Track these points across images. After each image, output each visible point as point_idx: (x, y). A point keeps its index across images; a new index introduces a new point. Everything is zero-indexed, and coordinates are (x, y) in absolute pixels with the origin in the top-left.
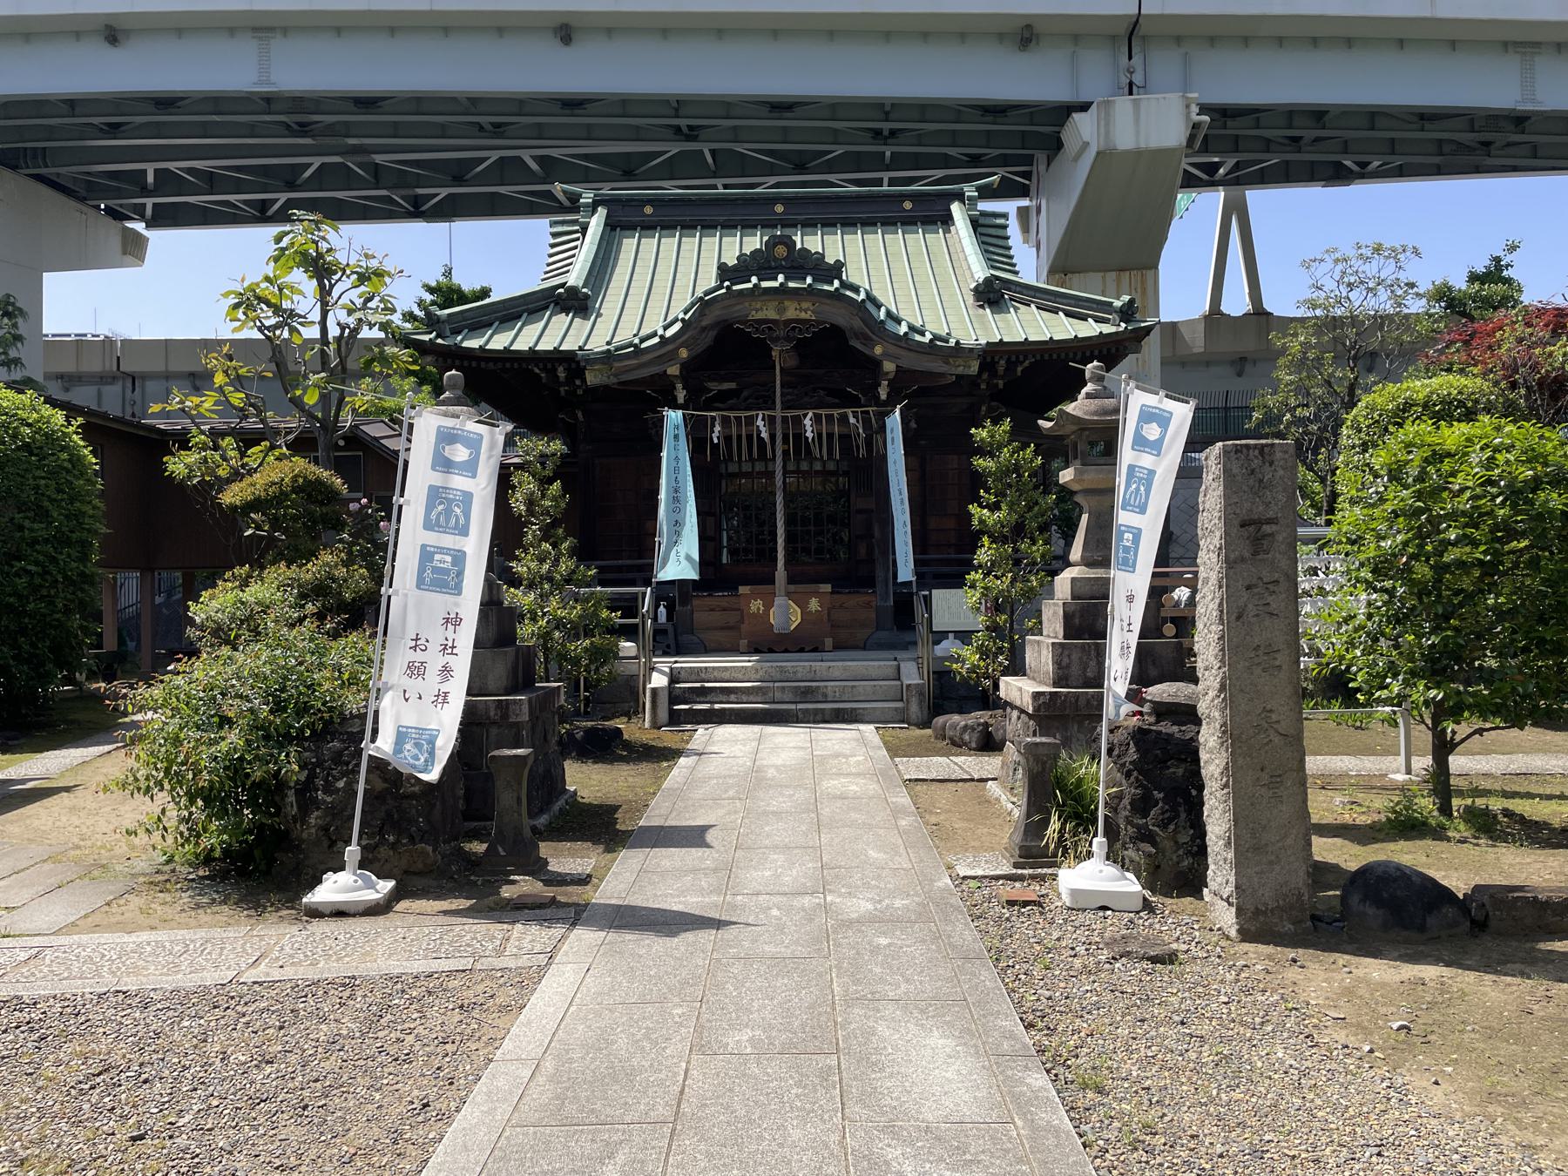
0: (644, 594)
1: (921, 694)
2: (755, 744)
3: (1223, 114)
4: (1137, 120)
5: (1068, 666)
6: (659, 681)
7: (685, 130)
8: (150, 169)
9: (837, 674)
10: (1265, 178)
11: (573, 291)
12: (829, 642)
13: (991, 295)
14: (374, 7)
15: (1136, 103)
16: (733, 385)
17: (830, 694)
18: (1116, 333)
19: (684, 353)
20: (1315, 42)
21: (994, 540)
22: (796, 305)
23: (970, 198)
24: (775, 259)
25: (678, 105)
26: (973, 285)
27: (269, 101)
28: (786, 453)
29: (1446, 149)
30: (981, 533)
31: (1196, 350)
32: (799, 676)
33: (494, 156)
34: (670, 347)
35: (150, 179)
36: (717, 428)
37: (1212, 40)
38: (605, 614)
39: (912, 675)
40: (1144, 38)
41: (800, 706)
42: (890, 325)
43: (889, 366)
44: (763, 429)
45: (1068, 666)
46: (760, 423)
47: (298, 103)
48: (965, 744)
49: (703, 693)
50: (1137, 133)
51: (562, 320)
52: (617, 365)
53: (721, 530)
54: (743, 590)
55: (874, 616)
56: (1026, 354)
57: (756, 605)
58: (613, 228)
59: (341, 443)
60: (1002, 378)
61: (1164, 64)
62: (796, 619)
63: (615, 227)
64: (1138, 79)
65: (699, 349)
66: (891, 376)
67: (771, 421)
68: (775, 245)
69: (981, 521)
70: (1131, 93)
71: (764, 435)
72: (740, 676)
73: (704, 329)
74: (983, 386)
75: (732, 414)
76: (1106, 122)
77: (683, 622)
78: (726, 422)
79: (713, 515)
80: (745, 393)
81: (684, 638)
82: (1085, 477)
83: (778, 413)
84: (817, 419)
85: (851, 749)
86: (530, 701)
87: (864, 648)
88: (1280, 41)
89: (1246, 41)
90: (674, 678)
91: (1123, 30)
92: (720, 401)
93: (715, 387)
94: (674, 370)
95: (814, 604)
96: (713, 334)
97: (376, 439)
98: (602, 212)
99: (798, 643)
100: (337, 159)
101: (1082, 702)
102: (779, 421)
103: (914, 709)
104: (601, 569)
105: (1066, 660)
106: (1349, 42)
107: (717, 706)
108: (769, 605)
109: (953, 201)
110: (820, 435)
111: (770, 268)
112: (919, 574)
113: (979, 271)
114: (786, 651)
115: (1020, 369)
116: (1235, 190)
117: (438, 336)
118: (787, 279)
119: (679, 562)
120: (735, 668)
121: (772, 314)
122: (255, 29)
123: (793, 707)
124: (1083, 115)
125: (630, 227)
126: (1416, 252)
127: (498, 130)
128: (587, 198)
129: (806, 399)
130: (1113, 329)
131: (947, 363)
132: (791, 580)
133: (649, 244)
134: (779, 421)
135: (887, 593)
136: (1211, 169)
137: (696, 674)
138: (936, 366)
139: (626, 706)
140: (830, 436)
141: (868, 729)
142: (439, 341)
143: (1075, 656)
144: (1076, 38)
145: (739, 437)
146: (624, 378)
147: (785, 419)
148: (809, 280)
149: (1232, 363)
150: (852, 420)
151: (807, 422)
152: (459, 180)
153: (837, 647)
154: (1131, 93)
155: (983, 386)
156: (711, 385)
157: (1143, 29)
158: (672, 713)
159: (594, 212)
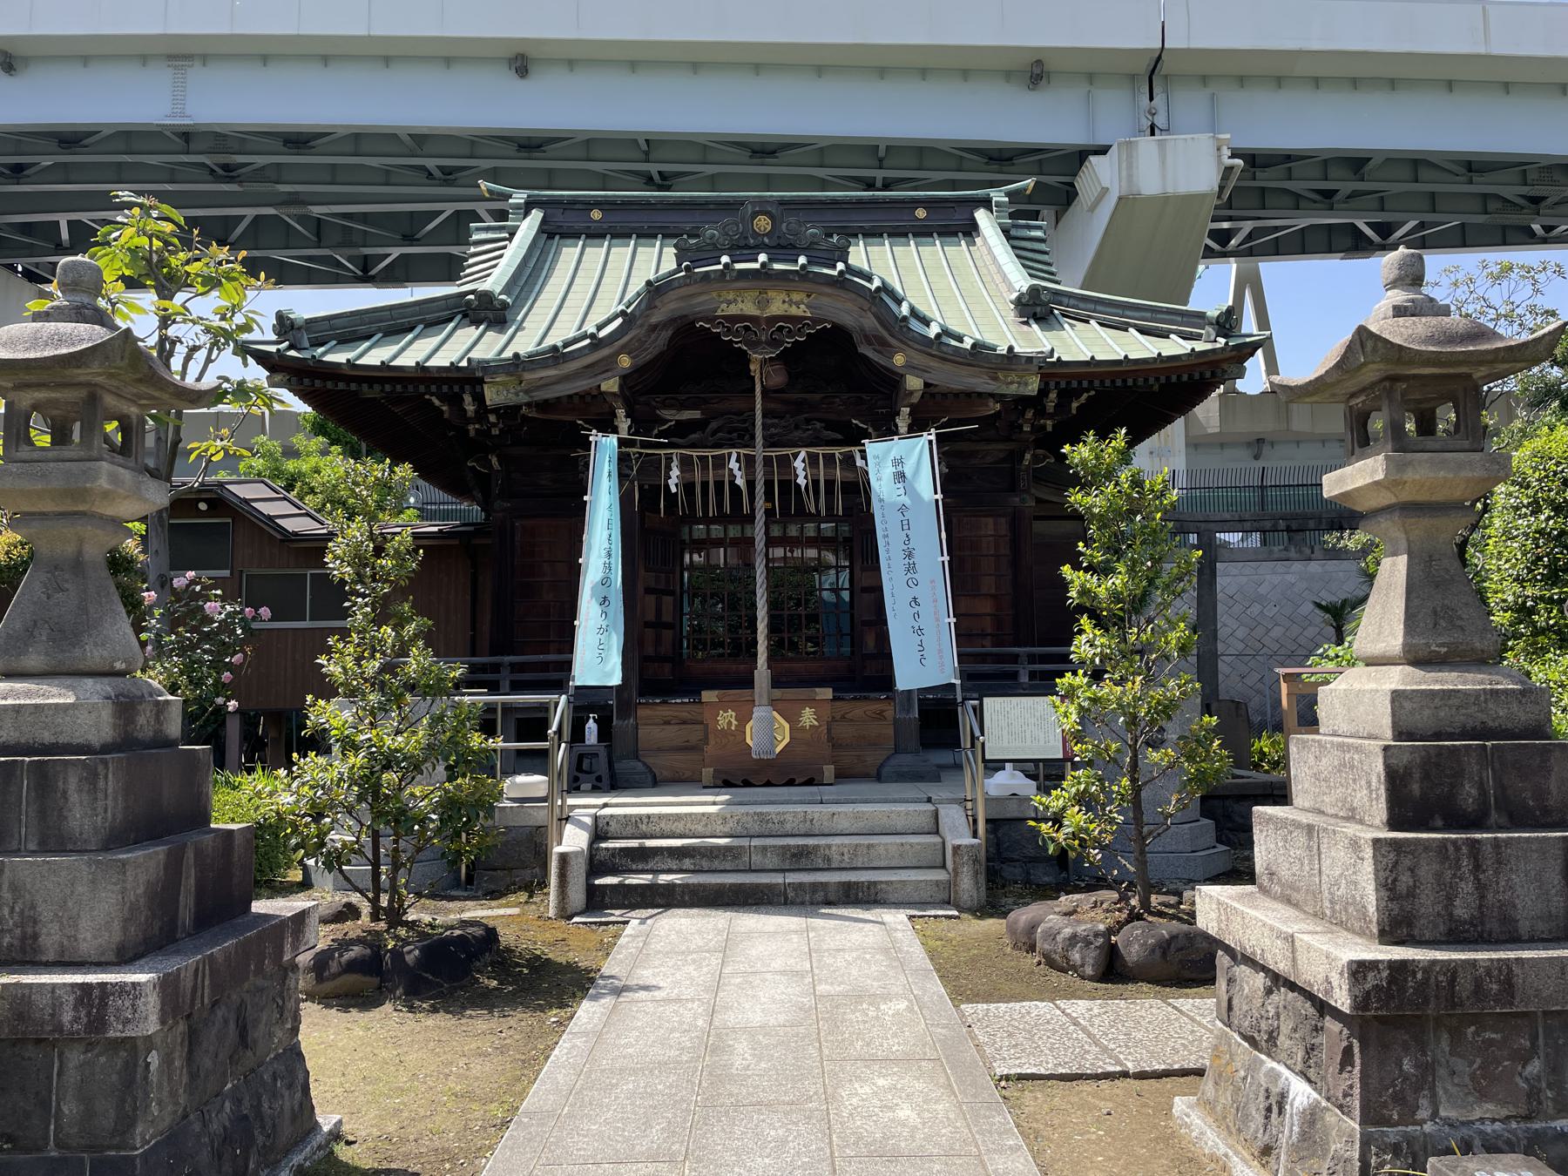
0: (557, 704)
1: (976, 861)
2: (715, 961)
3: (1255, 160)
5: (1411, 894)
6: (574, 840)
7: (656, 177)
8: (63, 220)
9: (843, 825)
10: (1281, 248)
11: (486, 297)
12: (829, 771)
13: (1035, 308)
15: (1161, 143)
16: (695, 414)
17: (836, 858)
18: (1213, 351)
19: (625, 362)
20: (1355, 83)
21: (1100, 623)
22: (783, 296)
23: (998, 204)
24: (755, 235)
25: (650, 145)
26: (1014, 296)
27: (186, 136)
28: (769, 513)
29: (1492, 206)
30: (1081, 609)
31: (1210, 431)
32: (788, 827)
33: (449, 208)
34: (605, 352)
35: (65, 235)
36: (675, 472)
37: (1242, 81)
38: (476, 740)
39: (959, 833)
41: (792, 878)
42: (915, 325)
43: (914, 383)
45: (1411, 894)
46: (733, 465)
47: (221, 139)
48: (1074, 968)
49: (643, 854)
50: (1164, 177)
51: (470, 333)
52: (527, 376)
53: (682, 614)
54: (708, 696)
55: (891, 731)
56: (1091, 377)
57: (726, 719)
58: (551, 236)
59: (203, 506)
60: (1051, 416)
61: (1187, 103)
62: (783, 740)
63: (551, 233)
64: (1160, 121)
65: (646, 357)
66: (915, 399)
67: (749, 462)
69: (1084, 592)
70: (1153, 134)
71: (740, 481)
72: (700, 828)
73: (654, 328)
74: (1027, 428)
75: (695, 453)
76: (1130, 163)
77: (611, 751)
78: (686, 463)
79: (672, 593)
80: (714, 425)
81: (622, 766)
82: (1410, 475)
83: (759, 452)
84: (812, 460)
85: (873, 953)
86: (168, 986)
87: (879, 778)
88: (1317, 82)
89: (1279, 81)
90: (599, 832)
91: (1143, 67)
92: (680, 434)
93: (672, 416)
94: (611, 385)
95: (808, 717)
97: (246, 501)
98: (536, 215)
100: (271, 211)
101: (1465, 986)
103: (969, 885)
104: (473, 668)
105: (1405, 880)
106: (1393, 84)
107: (664, 878)
108: (744, 719)
109: (977, 207)
110: (816, 483)
111: (747, 247)
112: (966, 676)
113: (1021, 281)
114: (768, 784)
115: (1075, 405)
116: (1248, 262)
117: (291, 347)
118: (771, 260)
119: (598, 657)
120: (693, 810)
121: (747, 307)
123: (777, 879)
124: (1101, 157)
125: (571, 235)
126: (1559, 272)
127: (449, 175)
128: (519, 197)
129: (797, 434)
130: (1209, 346)
131: (996, 379)
132: (776, 683)
133: (595, 253)
136: (1222, 237)
137: (635, 826)
138: (982, 383)
139: (526, 874)
140: (830, 484)
141: (897, 918)
142: (292, 353)
143: (1426, 871)
144: (1091, 77)
145: (705, 485)
147: (768, 461)
148: (802, 260)
149: (1249, 445)
151: (799, 464)
152: (409, 239)
153: (843, 776)
154: (1153, 134)
155: (1027, 428)
156: (666, 414)
157: (1165, 68)
158: (592, 890)
159: (526, 214)
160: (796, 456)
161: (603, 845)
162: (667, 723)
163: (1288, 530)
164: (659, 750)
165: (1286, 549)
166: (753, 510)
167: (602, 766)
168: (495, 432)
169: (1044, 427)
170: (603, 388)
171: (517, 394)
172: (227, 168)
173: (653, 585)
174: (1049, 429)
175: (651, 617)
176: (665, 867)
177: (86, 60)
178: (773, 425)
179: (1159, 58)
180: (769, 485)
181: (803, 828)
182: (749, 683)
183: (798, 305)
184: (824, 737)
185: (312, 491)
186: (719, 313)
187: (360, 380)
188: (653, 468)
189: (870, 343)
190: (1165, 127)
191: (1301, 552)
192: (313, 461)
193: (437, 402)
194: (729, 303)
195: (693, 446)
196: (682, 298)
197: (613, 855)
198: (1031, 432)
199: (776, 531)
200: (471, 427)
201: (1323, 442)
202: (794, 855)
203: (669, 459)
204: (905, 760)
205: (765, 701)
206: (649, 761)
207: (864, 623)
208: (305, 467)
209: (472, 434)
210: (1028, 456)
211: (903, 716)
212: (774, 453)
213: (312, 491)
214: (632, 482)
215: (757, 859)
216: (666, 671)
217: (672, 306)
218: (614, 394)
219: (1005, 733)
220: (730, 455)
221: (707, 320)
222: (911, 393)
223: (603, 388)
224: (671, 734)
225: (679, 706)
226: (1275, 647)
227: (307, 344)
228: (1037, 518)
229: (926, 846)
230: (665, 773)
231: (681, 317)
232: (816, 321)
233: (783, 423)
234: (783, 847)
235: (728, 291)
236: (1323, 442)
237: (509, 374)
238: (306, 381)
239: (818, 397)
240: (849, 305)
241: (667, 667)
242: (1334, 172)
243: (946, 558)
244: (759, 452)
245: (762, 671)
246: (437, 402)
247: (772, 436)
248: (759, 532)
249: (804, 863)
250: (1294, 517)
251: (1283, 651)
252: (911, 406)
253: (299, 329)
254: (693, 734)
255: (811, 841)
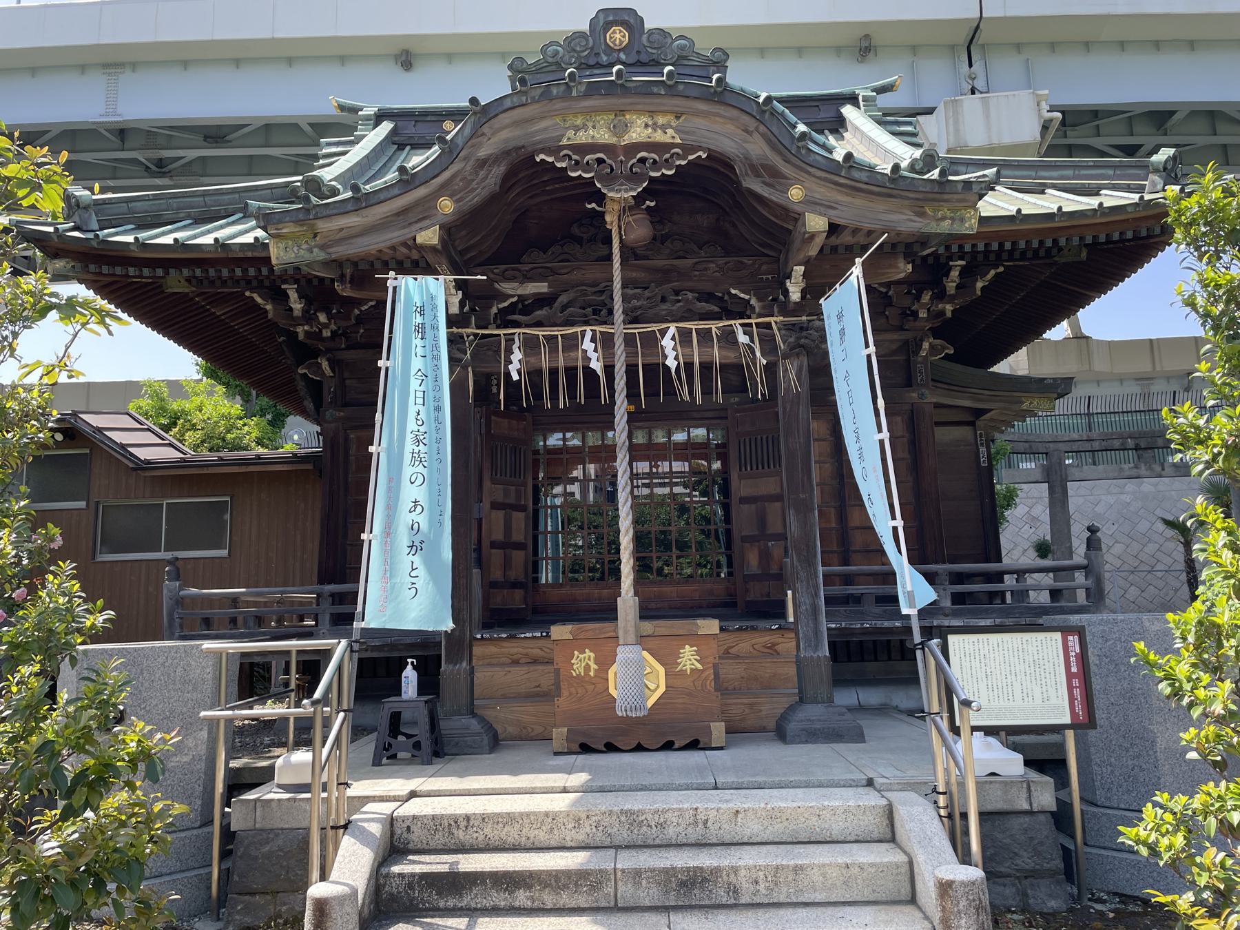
3: (1073, 117)
4: (987, 116)
9: (752, 828)
12: (718, 730)
14: (218, 36)
15: (985, 102)
16: (542, 288)
17: (746, 886)
19: (447, 206)
20: (1157, 45)
22: (646, 119)
23: (865, 99)
24: (609, 50)
27: (122, 133)
32: (671, 833)
36: (517, 356)
37: (1053, 46)
40: (983, 46)
43: (816, 223)
44: (593, 356)
46: (588, 345)
52: (323, 226)
54: (560, 632)
55: (792, 671)
57: (583, 661)
58: (401, 147)
60: (952, 299)
61: (1006, 67)
62: (657, 685)
64: (980, 84)
65: (476, 197)
67: (606, 343)
68: (608, 25)
70: (973, 93)
72: (542, 836)
73: (482, 163)
74: (923, 314)
75: (540, 332)
78: (530, 345)
79: (523, 508)
80: (563, 299)
81: (452, 725)
83: (618, 328)
84: (684, 338)
87: (781, 734)
89: (1087, 46)
90: (395, 845)
91: (963, 36)
93: (514, 290)
95: (689, 658)
96: (499, 170)
98: (386, 127)
99: (666, 734)
102: (619, 342)
108: (605, 661)
109: (843, 104)
114: (639, 748)
115: (979, 285)
117: (75, 229)
119: (406, 583)
122: (106, 66)
131: (922, 214)
132: (646, 613)
134: (619, 342)
135: (816, 632)
137: (452, 835)
140: (706, 367)
142: (76, 234)
144: (914, 49)
145: (554, 372)
146: (339, 251)
147: (629, 340)
150: (743, 339)
151: (667, 343)
156: (507, 287)
157: (982, 38)
159: (376, 125)
160: (663, 333)
161: (396, 869)
162: (516, 662)
163: (1137, 448)
164: (505, 697)
165: (1136, 467)
166: (613, 402)
167: (421, 731)
168: (326, 333)
169: (943, 313)
170: (419, 240)
171: (310, 250)
172: (160, 163)
173: (500, 499)
174: (949, 314)
175: (499, 536)
176: (487, 903)
177: (33, 71)
178: (635, 297)
179: (978, 27)
180: (631, 370)
181: (693, 835)
182: (608, 612)
183: (664, 128)
184: (710, 685)
185: (194, 427)
186: (565, 142)
187: (153, 263)
188: (490, 350)
189: (758, 175)
190: (985, 89)
191: (1150, 469)
192: (197, 400)
193: (259, 300)
194: (577, 129)
195: (538, 324)
196: (516, 124)
197: (411, 886)
198: (927, 320)
199: (640, 438)
200: (300, 329)
201: (1121, 381)
202: (682, 884)
203: (510, 340)
204: (813, 713)
205: (632, 637)
206: (489, 714)
207: (744, 539)
208: (188, 406)
209: (301, 337)
210: (926, 345)
211: (810, 654)
212: (637, 329)
213: (194, 427)
214: (465, 368)
215: (626, 892)
216: (516, 599)
217: (505, 134)
218: (433, 248)
219: (982, 686)
220: (583, 333)
221: (548, 151)
222: (813, 236)
223: (419, 240)
224: (519, 678)
225: (527, 641)
226: (1118, 563)
227: (96, 227)
228: (938, 424)
229: (882, 868)
230: (510, 729)
231: (518, 149)
232: (688, 149)
233: (647, 293)
234: (666, 871)
235: (575, 114)
236: (1121, 381)
237: (298, 222)
238: (92, 267)
239: (689, 262)
240: (730, 127)
241: (519, 594)
242: (1137, 128)
243: (885, 435)
244: (618, 328)
245: (627, 600)
246: (259, 300)
247: (635, 309)
248: (620, 433)
249: (697, 896)
250: (1142, 435)
251: (1126, 567)
252: (807, 263)
253: (86, 208)
254: (543, 677)
255: (705, 860)
